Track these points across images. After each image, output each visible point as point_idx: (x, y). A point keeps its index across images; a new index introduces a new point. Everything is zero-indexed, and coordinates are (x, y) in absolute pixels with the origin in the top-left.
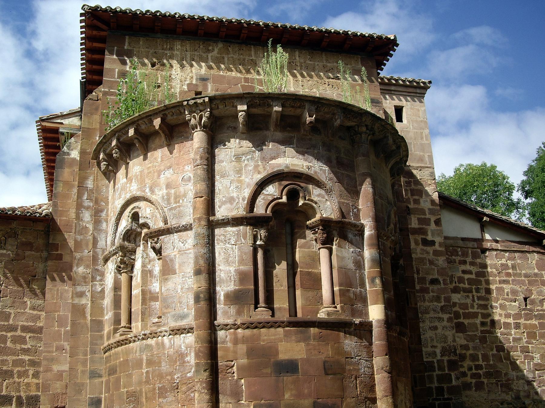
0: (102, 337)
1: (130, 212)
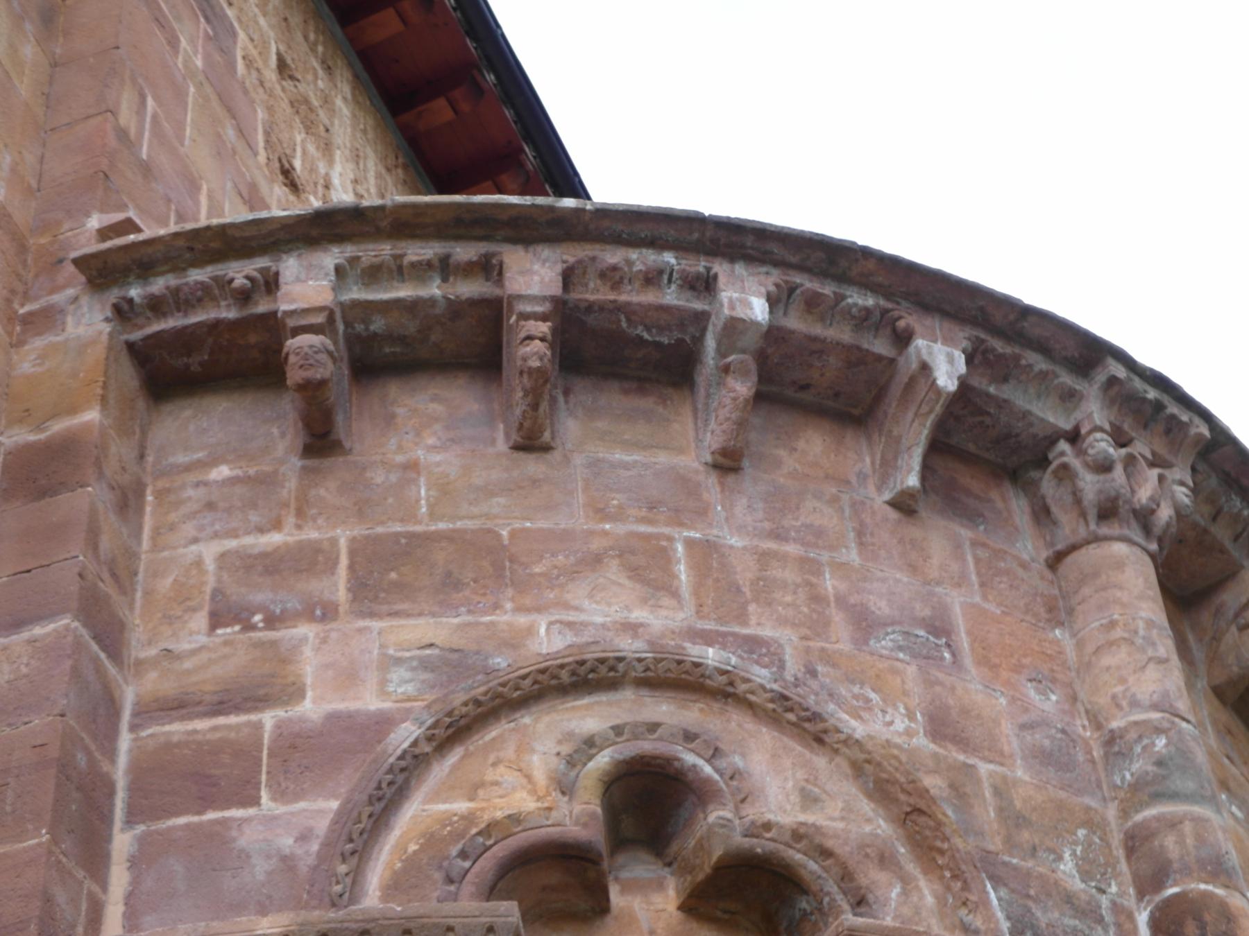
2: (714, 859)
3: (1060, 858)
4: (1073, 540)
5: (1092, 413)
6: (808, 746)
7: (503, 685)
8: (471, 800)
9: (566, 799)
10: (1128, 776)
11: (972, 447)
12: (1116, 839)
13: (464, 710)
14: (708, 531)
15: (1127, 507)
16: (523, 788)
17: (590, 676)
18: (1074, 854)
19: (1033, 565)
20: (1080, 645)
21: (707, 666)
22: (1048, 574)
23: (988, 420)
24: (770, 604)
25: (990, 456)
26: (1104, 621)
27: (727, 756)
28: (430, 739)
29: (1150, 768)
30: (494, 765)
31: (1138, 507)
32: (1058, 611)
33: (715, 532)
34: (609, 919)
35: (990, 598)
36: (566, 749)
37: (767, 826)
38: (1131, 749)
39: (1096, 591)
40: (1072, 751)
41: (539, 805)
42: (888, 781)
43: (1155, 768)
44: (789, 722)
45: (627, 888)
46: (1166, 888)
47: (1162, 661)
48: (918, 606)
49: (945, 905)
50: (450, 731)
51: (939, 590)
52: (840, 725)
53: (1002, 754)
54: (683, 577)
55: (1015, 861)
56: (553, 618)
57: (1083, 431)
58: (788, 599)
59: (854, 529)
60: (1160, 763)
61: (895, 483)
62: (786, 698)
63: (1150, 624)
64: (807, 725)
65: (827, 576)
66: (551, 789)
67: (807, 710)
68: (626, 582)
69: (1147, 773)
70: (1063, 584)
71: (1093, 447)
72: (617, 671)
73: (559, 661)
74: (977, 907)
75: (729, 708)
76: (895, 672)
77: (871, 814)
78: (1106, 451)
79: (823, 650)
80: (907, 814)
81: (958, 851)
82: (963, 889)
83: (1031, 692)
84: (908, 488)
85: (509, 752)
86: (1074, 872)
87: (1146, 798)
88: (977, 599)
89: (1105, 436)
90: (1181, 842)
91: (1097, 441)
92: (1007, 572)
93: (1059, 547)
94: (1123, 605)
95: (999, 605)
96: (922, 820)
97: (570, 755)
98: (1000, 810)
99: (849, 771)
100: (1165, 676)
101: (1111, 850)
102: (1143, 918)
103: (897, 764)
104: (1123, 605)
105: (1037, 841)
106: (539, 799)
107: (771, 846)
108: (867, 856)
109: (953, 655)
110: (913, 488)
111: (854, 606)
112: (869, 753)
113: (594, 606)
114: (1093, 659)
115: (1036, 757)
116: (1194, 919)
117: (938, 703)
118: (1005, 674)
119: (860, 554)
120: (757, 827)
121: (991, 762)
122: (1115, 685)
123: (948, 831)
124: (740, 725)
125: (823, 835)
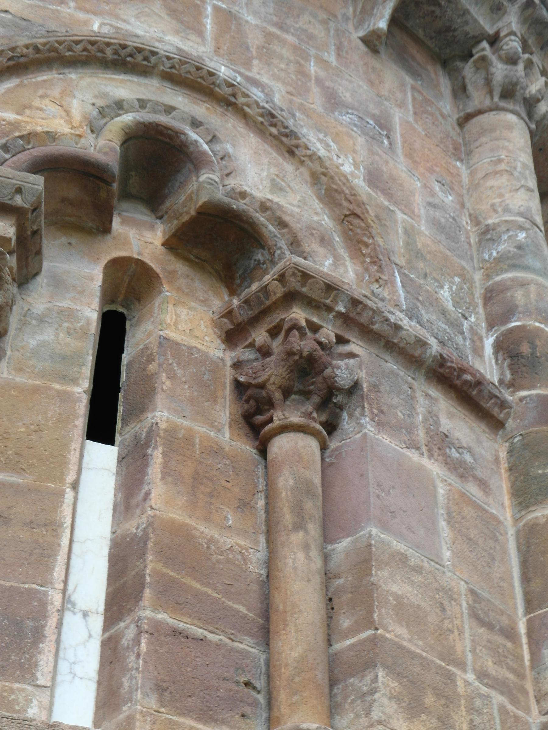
2: (200, 203)
3: (442, 287)
4: (479, 107)
5: (511, 22)
6: (282, 155)
7: (60, 43)
8: (18, 114)
9: (94, 136)
10: (494, 254)
11: (420, 33)
12: (478, 292)
13: (25, 51)
14: (231, 6)
15: (522, 91)
16: (61, 117)
17: (129, 59)
18: (451, 288)
19: (449, 119)
20: (472, 174)
21: (219, 76)
22: (457, 129)
23: (438, 12)
24: (269, 65)
25: (431, 44)
26: (493, 159)
27: (221, 142)
29: (512, 249)
30: (42, 97)
31: (528, 96)
32: (463, 151)
33: (237, 8)
34: (108, 237)
35: (419, 123)
36: (100, 103)
37: (243, 195)
38: (500, 237)
39: (491, 140)
40: (458, 232)
41: (73, 131)
42: (336, 191)
43: (515, 250)
44: (271, 134)
45: (124, 222)
46: (511, 322)
47: (529, 190)
48: (371, 106)
49: (362, 281)
50: (11, 63)
51: (386, 103)
52: (309, 145)
53: (413, 212)
54: (209, 27)
55: (412, 276)
56: (106, 21)
57: (502, 34)
58: (283, 66)
59: (335, 44)
60: (519, 247)
61: (369, 25)
62: (273, 116)
63: (525, 166)
64: (284, 139)
65: (312, 64)
66: (83, 124)
67: (286, 127)
68: (166, 17)
69: (509, 252)
70: (467, 136)
71: (507, 45)
72: (149, 62)
73: (107, 40)
74: (386, 284)
75: (229, 114)
76: (350, 136)
77: (319, 210)
78: (517, 48)
79: (302, 104)
80: (346, 216)
81: (379, 246)
82: (378, 271)
83: (437, 187)
84: (378, 29)
85: (56, 92)
86: (449, 299)
87: (506, 267)
88: (411, 119)
89: (517, 39)
90: (527, 295)
91: (511, 40)
92: (432, 115)
93: (469, 110)
94: (509, 151)
95: (425, 130)
96: (356, 221)
97: (102, 108)
98: (407, 244)
99: (309, 179)
100: (530, 199)
101: (474, 298)
102: (489, 342)
103: (345, 181)
104: (509, 151)
105: (428, 271)
106: (73, 128)
107: (245, 207)
108: (312, 234)
109: (390, 144)
110: (382, 29)
111: (328, 88)
112: (327, 169)
113: (138, 23)
114: (482, 181)
115: (435, 225)
116: (528, 342)
117: (376, 166)
118: (422, 170)
119: (337, 60)
120: (235, 193)
121: (405, 214)
122: (495, 198)
123: (374, 232)
124: (234, 127)
125: (283, 212)
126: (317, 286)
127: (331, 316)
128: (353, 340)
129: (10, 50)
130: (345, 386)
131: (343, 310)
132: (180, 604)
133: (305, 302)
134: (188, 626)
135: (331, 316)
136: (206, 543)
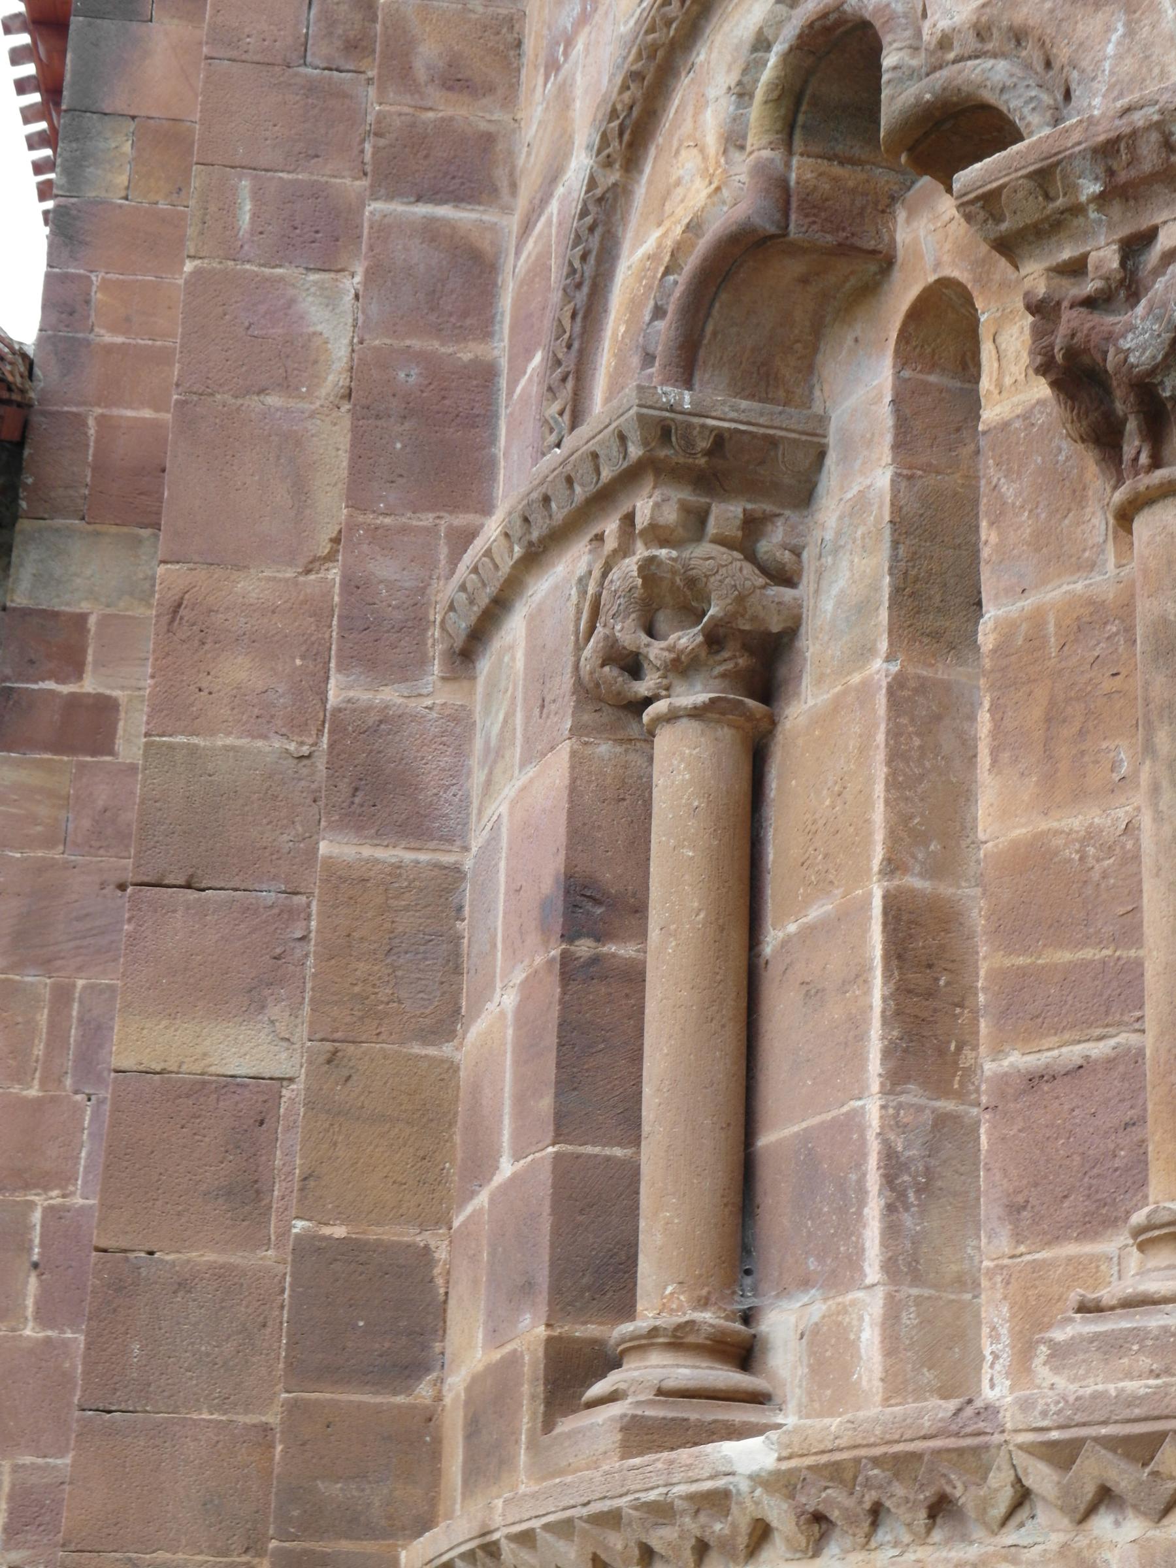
0: (416, 1441)
1: (743, 93)
13: (627, 96)
28: (608, 163)
126: (1020, 195)
127: (1093, 215)
128: (1157, 220)
129: (610, 121)
130: (1154, 357)
131: (1096, 188)
132: (1037, 1017)
133: (1031, 238)
134: (1056, 1053)
135: (1093, 215)
136: (1077, 852)
